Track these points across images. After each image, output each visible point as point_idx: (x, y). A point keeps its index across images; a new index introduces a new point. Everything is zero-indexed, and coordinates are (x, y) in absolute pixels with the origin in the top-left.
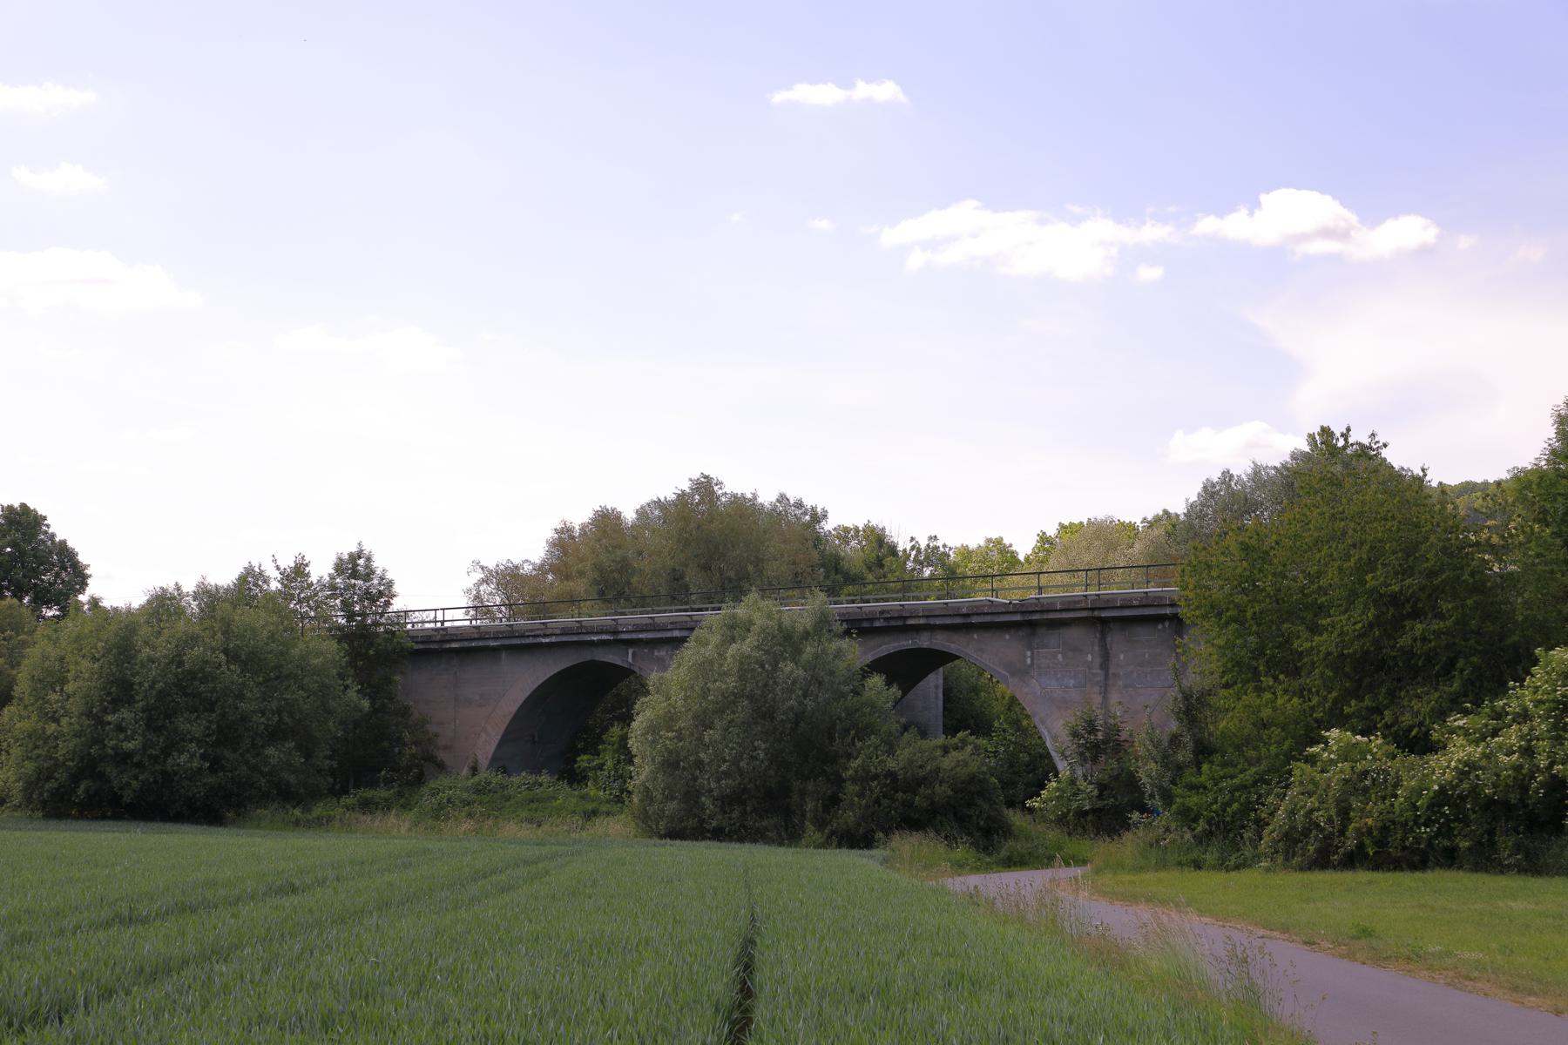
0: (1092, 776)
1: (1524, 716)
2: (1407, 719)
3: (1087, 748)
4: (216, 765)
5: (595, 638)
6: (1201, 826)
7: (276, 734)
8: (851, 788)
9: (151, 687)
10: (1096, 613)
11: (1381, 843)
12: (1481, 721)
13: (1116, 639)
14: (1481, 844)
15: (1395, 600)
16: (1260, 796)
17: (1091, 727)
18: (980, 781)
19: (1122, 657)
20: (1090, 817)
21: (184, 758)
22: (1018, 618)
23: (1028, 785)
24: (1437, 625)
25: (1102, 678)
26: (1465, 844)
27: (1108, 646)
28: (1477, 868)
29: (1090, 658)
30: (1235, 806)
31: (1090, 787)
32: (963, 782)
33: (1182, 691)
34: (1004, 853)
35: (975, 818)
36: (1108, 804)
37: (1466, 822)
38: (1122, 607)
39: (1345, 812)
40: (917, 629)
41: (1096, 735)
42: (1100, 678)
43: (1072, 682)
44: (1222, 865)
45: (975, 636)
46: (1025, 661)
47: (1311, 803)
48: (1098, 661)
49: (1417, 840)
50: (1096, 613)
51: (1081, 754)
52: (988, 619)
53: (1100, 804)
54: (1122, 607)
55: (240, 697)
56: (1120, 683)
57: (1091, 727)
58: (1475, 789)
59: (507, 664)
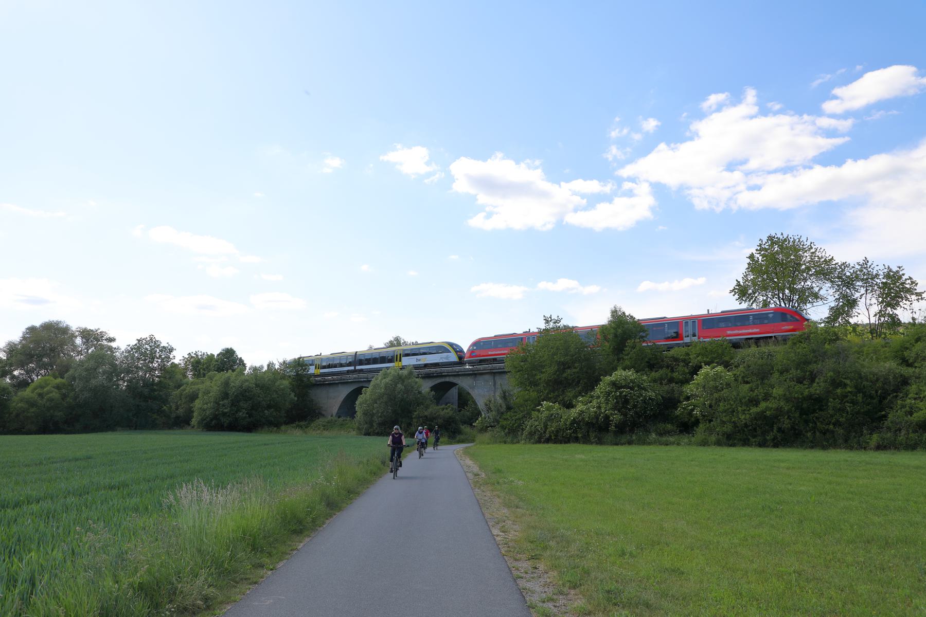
1: (598, 397)
2: (566, 399)
4: (250, 416)
5: (362, 380)
6: (507, 431)
7: (269, 407)
8: (415, 420)
9: (233, 394)
10: (492, 371)
11: (556, 436)
12: (586, 399)
13: (497, 378)
14: (585, 435)
15: (563, 364)
16: (523, 421)
21: (241, 414)
22: (471, 372)
24: (574, 370)
26: (580, 435)
28: (584, 443)
30: (516, 424)
33: (503, 391)
34: (458, 439)
37: (581, 429)
38: (499, 369)
39: (546, 427)
40: (445, 376)
42: (493, 389)
43: (486, 390)
44: (512, 442)
47: (537, 423)
49: (567, 434)
50: (492, 371)
51: (488, 410)
54: (499, 369)
55: (259, 396)
58: (583, 419)
59: (340, 388)
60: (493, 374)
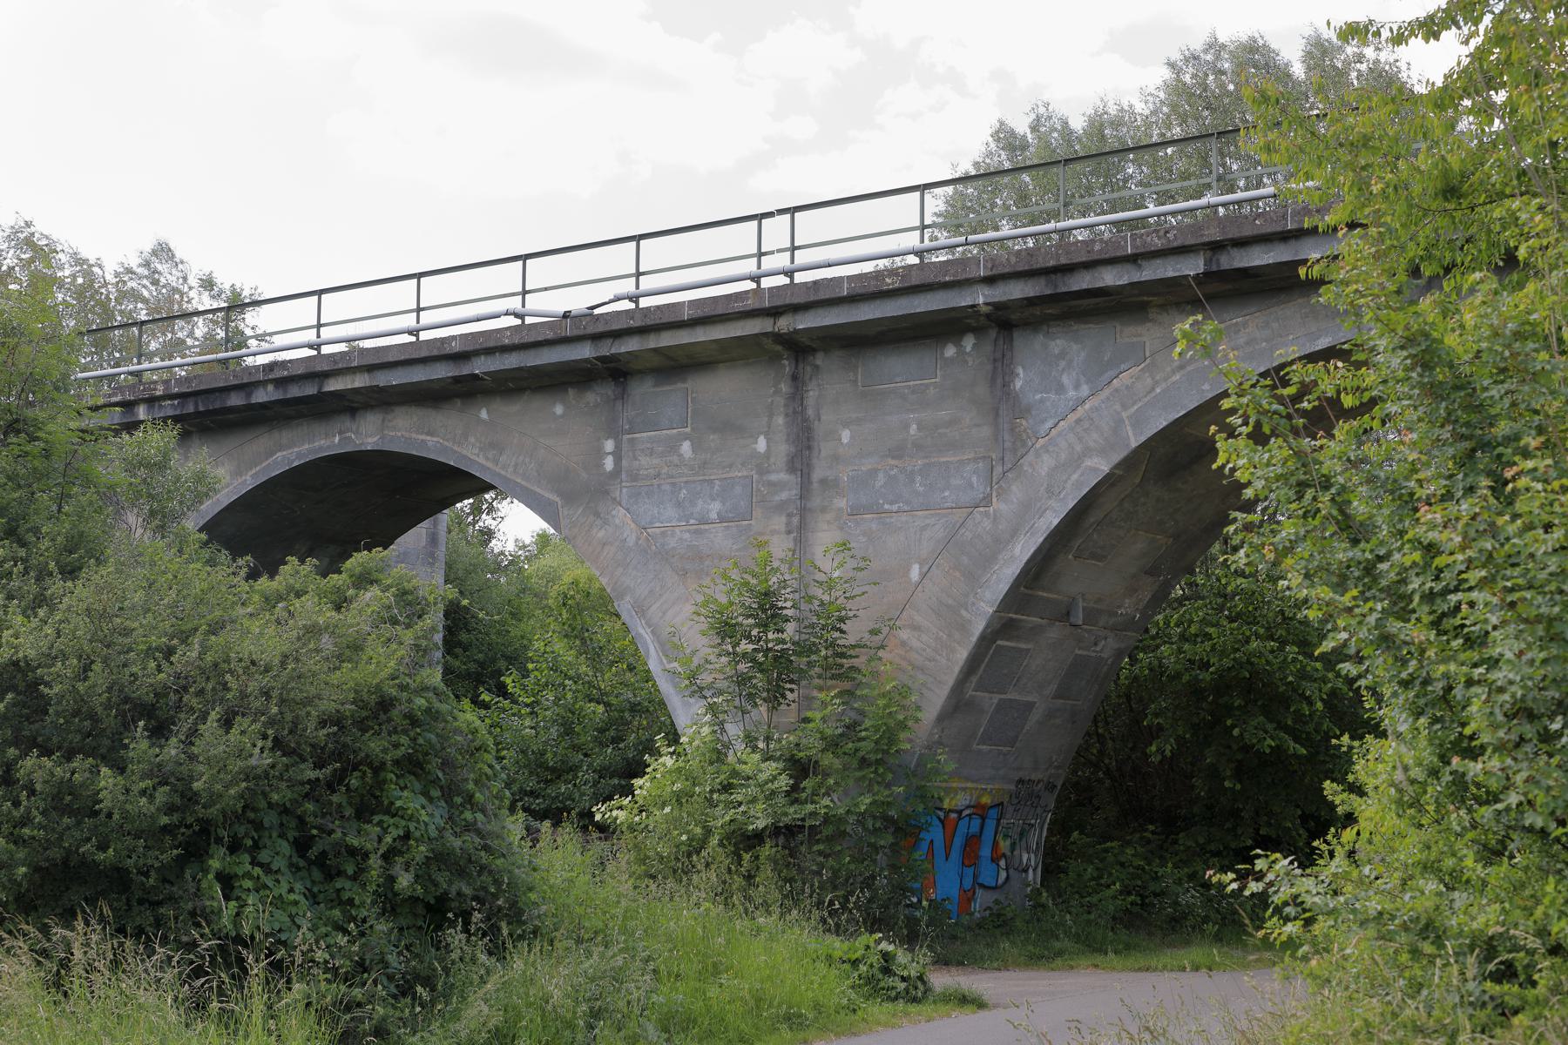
0: (768, 739)
3: (759, 667)
10: (784, 324)
17: (768, 610)
18: (413, 721)
19: (846, 436)
20: (767, 850)
22: (585, 352)
23: (602, 773)
25: (795, 492)
27: (810, 412)
29: (761, 445)
31: (772, 767)
32: (337, 720)
35: (375, 862)
36: (813, 814)
41: (782, 631)
45: (484, 414)
46: (600, 465)
48: (783, 449)
51: (742, 680)
52: (511, 361)
53: (793, 813)
56: (841, 503)
57: (768, 610)
60: (787, 366)
